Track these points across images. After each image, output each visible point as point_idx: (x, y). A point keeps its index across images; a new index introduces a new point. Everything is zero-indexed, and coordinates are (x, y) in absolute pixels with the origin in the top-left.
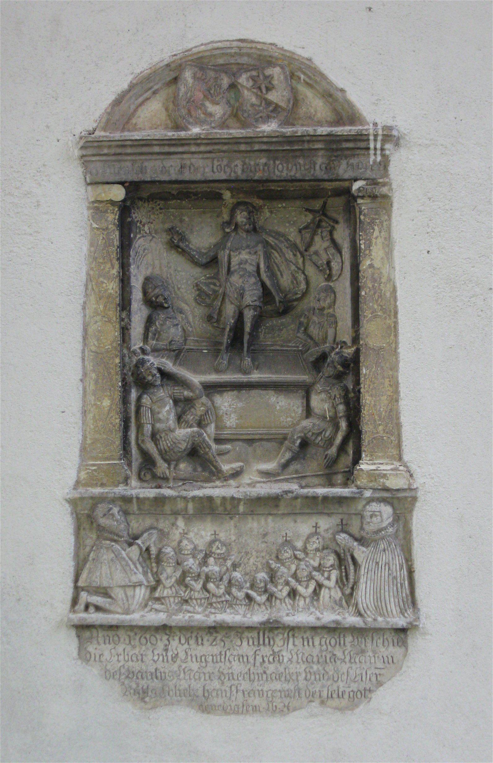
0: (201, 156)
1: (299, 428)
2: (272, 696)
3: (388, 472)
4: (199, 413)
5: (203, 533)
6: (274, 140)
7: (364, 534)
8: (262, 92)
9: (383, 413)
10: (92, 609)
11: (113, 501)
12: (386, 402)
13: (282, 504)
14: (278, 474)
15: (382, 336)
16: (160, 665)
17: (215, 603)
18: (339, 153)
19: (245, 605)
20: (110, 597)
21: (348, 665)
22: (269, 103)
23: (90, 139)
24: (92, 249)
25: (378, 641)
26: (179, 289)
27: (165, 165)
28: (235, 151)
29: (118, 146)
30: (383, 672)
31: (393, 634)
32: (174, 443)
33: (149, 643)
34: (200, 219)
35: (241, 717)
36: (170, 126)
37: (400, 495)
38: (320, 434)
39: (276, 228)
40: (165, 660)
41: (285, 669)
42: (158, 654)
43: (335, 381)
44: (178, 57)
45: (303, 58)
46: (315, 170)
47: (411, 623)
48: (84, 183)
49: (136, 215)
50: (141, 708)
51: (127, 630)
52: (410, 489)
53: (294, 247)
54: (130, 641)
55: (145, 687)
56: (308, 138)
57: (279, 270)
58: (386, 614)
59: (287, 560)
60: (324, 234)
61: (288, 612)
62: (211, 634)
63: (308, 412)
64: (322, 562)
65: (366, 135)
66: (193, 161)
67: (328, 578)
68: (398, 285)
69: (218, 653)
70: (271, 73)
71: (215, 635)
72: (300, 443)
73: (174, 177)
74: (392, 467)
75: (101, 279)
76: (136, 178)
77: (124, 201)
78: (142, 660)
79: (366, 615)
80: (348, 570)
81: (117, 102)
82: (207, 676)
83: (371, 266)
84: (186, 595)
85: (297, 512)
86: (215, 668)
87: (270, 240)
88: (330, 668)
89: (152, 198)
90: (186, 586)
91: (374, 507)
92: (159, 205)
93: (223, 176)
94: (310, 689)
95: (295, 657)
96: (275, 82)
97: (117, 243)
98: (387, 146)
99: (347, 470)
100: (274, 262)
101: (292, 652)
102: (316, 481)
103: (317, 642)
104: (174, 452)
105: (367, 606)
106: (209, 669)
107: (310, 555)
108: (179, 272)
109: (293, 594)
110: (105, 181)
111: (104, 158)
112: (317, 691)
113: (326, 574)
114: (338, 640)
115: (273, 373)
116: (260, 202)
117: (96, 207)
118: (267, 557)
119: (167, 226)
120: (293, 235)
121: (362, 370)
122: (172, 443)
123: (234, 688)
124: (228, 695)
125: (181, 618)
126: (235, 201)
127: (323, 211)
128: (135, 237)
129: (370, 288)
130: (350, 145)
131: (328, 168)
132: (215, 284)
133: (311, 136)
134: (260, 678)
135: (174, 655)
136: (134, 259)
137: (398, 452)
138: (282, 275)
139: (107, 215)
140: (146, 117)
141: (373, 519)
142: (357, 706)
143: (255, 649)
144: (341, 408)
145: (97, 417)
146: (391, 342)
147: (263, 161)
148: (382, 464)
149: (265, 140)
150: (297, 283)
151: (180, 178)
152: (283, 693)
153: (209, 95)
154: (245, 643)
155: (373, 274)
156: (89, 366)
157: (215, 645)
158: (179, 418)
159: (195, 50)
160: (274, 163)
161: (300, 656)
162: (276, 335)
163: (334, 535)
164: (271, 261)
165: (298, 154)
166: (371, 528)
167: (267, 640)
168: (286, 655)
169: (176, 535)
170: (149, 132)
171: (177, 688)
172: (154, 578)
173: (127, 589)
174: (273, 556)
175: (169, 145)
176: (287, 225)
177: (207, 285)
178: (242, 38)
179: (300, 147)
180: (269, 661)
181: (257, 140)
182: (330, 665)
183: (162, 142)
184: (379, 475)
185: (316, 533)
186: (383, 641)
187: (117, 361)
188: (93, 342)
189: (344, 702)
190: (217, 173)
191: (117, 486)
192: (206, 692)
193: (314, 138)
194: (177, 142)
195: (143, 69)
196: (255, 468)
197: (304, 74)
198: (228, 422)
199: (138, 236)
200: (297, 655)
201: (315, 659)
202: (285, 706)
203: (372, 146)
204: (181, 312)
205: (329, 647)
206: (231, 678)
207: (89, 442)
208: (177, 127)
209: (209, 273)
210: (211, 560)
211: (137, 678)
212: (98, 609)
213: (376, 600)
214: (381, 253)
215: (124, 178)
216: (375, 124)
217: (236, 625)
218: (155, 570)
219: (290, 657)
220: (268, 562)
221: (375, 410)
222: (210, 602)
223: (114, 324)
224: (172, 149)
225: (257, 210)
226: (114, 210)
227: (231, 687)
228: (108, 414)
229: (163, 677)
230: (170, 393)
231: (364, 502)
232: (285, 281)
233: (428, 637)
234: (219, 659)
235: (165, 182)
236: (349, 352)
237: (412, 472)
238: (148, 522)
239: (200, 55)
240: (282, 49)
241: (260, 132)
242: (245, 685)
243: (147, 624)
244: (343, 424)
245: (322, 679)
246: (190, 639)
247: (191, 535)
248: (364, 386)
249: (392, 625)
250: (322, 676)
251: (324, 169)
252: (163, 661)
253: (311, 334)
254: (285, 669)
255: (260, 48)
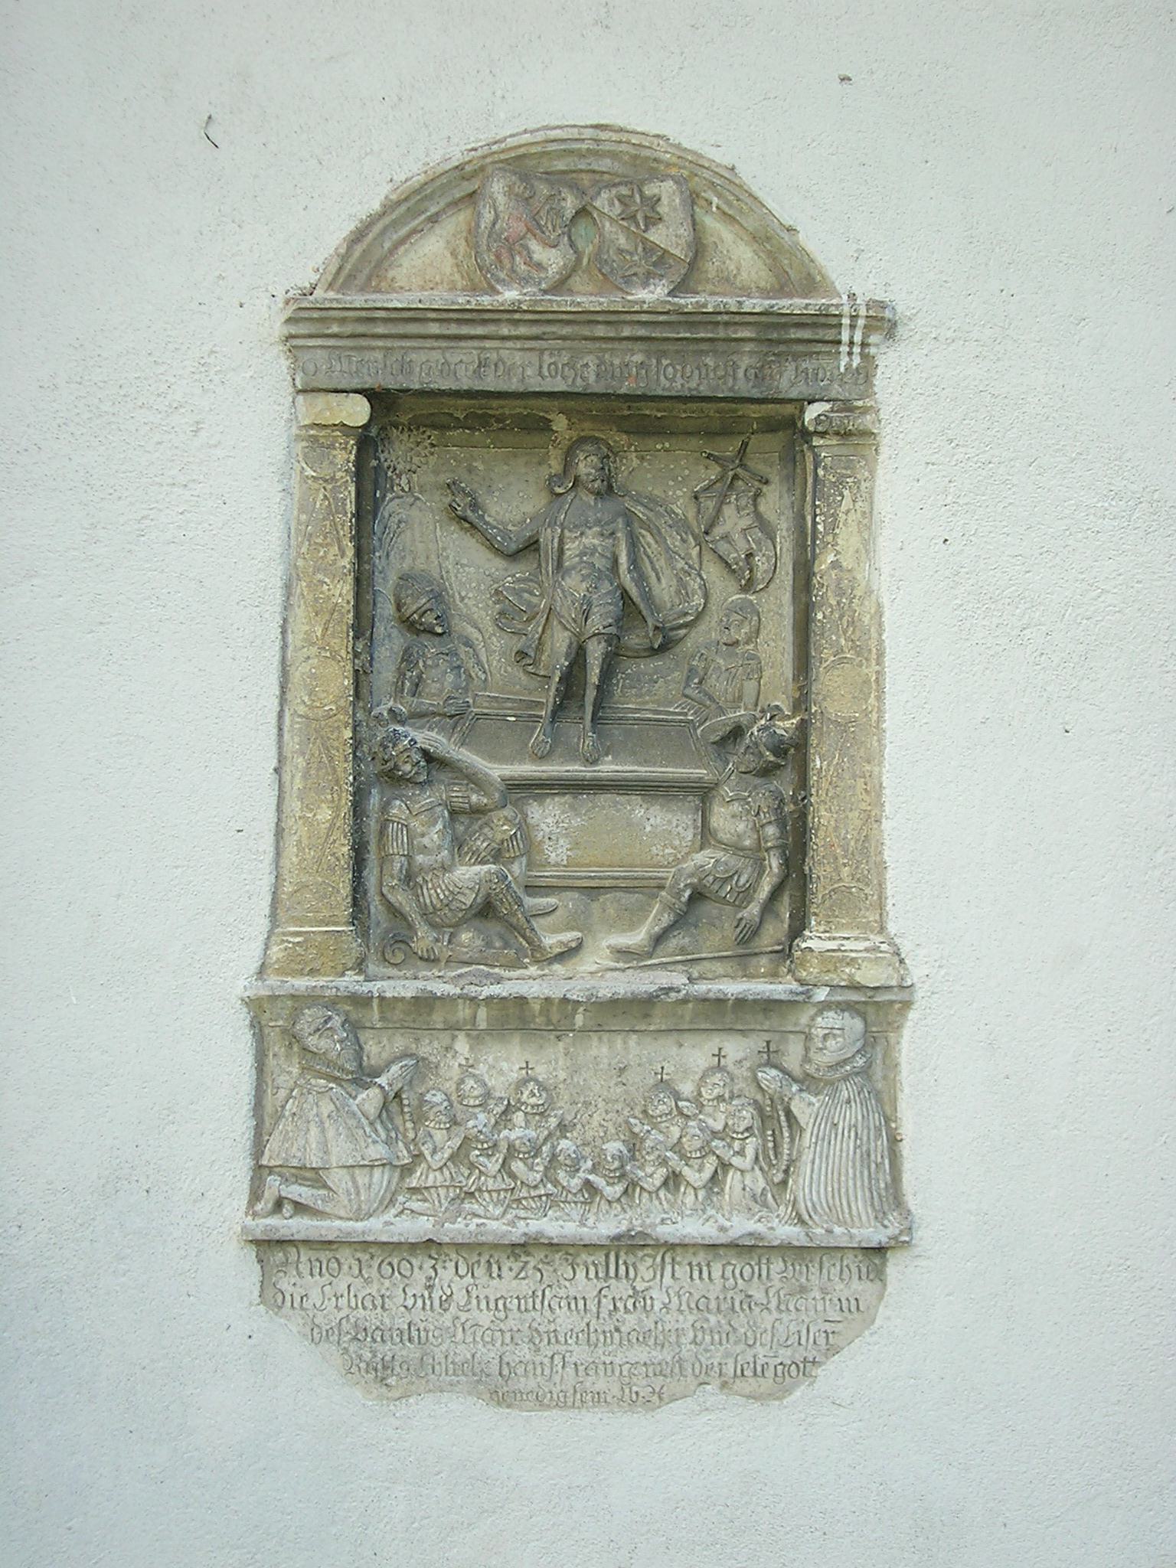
0: (519, 345)
1: (688, 865)
2: (631, 1375)
3: (860, 955)
4: (499, 837)
5: (505, 1065)
6: (661, 318)
7: (810, 1069)
8: (638, 225)
9: (852, 843)
10: (287, 1209)
11: (332, 1003)
12: (858, 823)
13: (657, 1011)
14: (650, 955)
15: (854, 698)
16: (417, 1315)
17: (525, 1198)
18: (782, 348)
19: (582, 1203)
20: (325, 1186)
21: (776, 1315)
22: (649, 248)
23: (305, 305)
24: (304, 517)
25: (833, 1270)
26: (462, 599)
27: (450, 359)
28: (586, 339)
29: (359, 320)
30: (838, 1327)
31: (860, 1257)
32: (452, 892)
33: (396, 1273)
34: (506, 468)
35: (571, 1413)
36: (459, 285)
37: (881, 997)
38: (726, 880)
39: (650, 489)
40: (428, 1307)
41: (656, 1323)
42: (414, 1295)
43: (758, 781)
44: (480, 153)
45: (719, 165)
46: (735, 379)
47: (895, 1238)
48: (291, 390)
49: (386, 454)
50: (380, 1397)
51: (356, 1250)
52: (902, 987)
53: (682, 525)
54: (360, 1271)
55: (387, 1358)
56: (726, 318)
57: (654, 569)
58: (849, 1220)
59: (664, 1119)
60: (743, 502)
61: (665, 1216)
62: (517, 1257)
63: (706, 835)
64: (730, 1123)
65: (835, 315)
66: (504, 353)
67: (741, 1153)
68: (885, 601)
69: (530, 1293)
70: (656, 191)
71: (524, 1258)
72: (690, 897)
73: (465, 384)
74: (867, 944)
75: (320, 576)
76: (391, 383)
77: (365, 427)
78: (383, 1307)
79: (810, 1223)
80: (778, 1138)
81: (357, 237)
82: (508, 1335)
83: (835, 565)
84: (471, 1184)
85: (686, 1027)
86: (523, 1321)
87: (639, 511)
88: (741, 1321)
89: (417, 424)
90: (472, 1166)
91: (831, 1019)
92: (429, 437)
93: (560, 386)
94: (703, 1360)
95: (675, 1300)
96: (663, 209)
97: (351, 507)
98: (873, 339)
99: (780, 947)
100: (645, 552)
101: (670, 1291)
102: (719, 968)
103: (717, 1273)
104: (450, 910)
105: (814, 1205)
106: (511, 1323)
107: (706, 1108)
108: (463, 566)
109: (673, 1181)
110: (331, 386)
111: (331, 342)
112: (716, 1364)
113: (737, 1145)
114: (756, 1268)
115: (640, 764)
116: (623, 439)
117: (312, 436)
118: (626, 1113)
119: (446, 478)
120: (682, 505)
121: (814, 761)
122: (447, 893)
123: (557, 1359)
124: (547, 1372)
125: (460, 1228)
126: (575, 435)
127: (741, 460)
128: (385, 496)
129: (831, 606)
130: (806, 334)
131: (759, 378)
132: (532, 594)
133: (733, 313)
134: (609, 1340)
135: (444, 1298)
136: (380, 540)
137: (877, 917)
138: (659, 579)
139: (335, 452)
140: (414, 267)
141: (828, 1044)
142: (788, 1391)
143: (599, 1287)
144: (771, 830)
145: (305, 842)
146: (870, 709)
147: (638, 358)
148: (848, 938)
149: (644, 318)
150: (687, 593)
151: (478, 386)
152: (651, 1369)
153: (535, 228)
154: (581, 1274)
155: (839, 580)
156: (292, 743)
157: (524, 1278)
158: (458, 844)
159: (511, 142)
160: (659, 362)
161: (684, 1299)
162: (644, 690)
163: (753, 1072)
164: (639, 550)
165: (704, 346)
166: (825, 1059)
167: (622, 1269)
168: (659, 1297)
169: (452, 1068)
170: (419, 295)
171: (450, 1360)
172: (409, 1152)
173: (357, 1171)
174: (637, 1112)
175: (458, 321)
176: (671, 483)
177: (518, 593)
178: (602, 122)
179: (710, 335)
180: (625, 1307)
181: (628, 317)
182: (742, 1315)
183: (445, 315)
184: (842, 960)
185: (719, 1068)
186: (842, 1271)
187: (348, 733)
188: (299, 696)
189: (766, 1384)
190: (549, 379)
191: (343, 974)
192: (505, 1366)
193: (737, 318)
194: (474, 316)
195: (410, 175)
196: (604, 944)
197: (720, 196)
198: (554, 854)
199: (389, 496)
200: (679, 1297)
201: (713, 1305)
202: (654, 1392)
203: (845, 337)
204: (468, 643)
205: (740, 1281)
206: (553, 1340)
207: (288, 888)
208: (474, 289)
209: (521, 570)
210: (519, 1118)
211: (374, 1340)
212: (300, 1208)
213: (830, 1194)
214: (855, 541)
215: (369, 383)
216: (852, 296)
217: (566, 1241)
218: (411, 1135)
219: (667, 1301)
220: (627, 1122)
221: (837, 837)
222: (516, 1197)
223: (342, 664)
224: (465, 330)
225: (616, 454)
226: (347, 443)
227: (552, 1357)
228: (328, 836)
229: (423, 1340)
230: (444, 797)
231: (812, 1011)
232: (664, 589)
233: (923, 1263)
234: (531, 1304)
235: (442, 393)
236: (786, 727)
237: (903, 956)
238: (400, 1043)
239: (522, 151)
240: (678, 146)
241: (636, 302)
242: (580, 1353)
243: (395, 1239)
244: (774, 863)
245: (724, 1342)
246: (476, 1266)
247: (481, 1069)
248: (817, 791)
249: (860, 1242)
250: (724, 1336)
251: (752, 377)
252: (424, 1308)
253: (711, 691)
254: (656, 1323)
255: (637, 142)
